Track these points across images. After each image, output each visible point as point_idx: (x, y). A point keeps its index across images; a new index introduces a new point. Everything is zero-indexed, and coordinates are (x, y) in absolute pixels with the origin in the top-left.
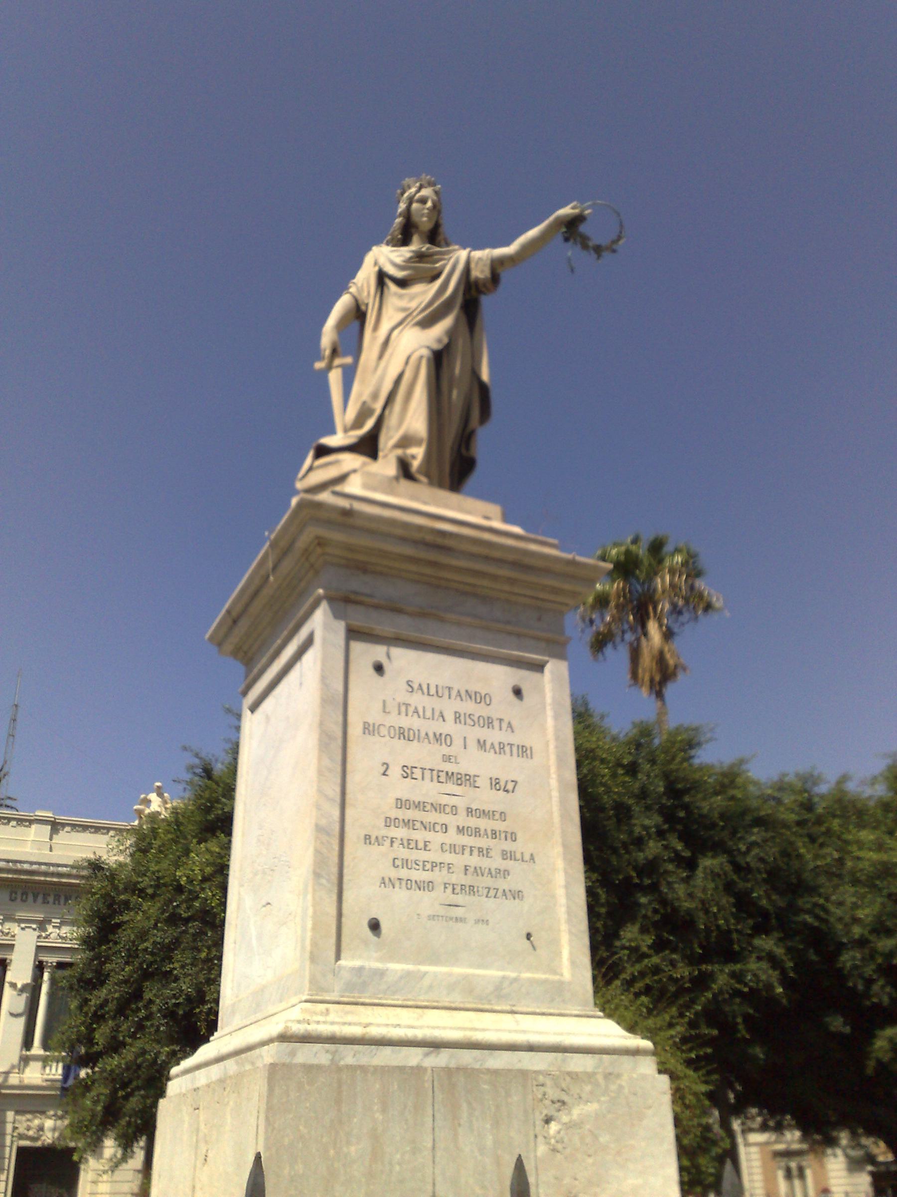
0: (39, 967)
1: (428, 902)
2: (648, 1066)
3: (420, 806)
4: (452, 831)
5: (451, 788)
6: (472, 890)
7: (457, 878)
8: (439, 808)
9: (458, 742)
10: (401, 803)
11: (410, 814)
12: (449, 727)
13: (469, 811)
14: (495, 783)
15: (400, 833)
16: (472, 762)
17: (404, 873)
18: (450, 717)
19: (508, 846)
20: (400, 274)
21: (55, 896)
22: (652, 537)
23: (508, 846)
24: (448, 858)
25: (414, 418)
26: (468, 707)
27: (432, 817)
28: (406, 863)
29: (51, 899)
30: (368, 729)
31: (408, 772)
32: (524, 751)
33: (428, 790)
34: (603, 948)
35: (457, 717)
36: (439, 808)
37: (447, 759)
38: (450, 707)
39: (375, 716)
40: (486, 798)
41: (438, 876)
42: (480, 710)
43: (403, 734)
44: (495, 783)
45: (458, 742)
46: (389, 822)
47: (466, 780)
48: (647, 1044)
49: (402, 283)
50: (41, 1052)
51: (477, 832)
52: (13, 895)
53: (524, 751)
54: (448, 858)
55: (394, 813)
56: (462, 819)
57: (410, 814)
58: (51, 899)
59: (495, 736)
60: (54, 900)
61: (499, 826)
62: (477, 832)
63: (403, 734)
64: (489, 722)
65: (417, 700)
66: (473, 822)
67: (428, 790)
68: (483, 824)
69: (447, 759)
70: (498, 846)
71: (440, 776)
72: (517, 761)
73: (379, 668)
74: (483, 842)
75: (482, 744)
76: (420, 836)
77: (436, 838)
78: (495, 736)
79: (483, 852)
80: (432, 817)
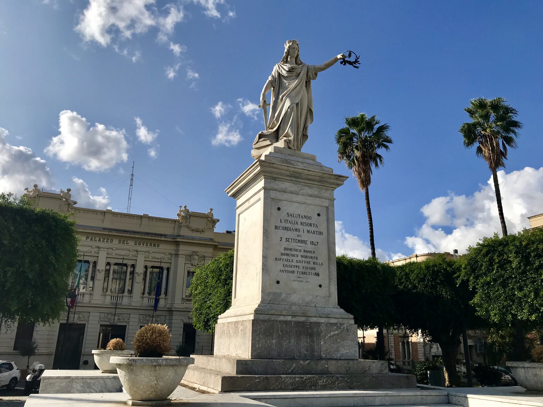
2: (352, 322)
3: (291, 250)
4: (300, 256)
5: (299, 244)
7: (301, 270)
8: (296, 250)
9: (302, 231)
11: (289, 252)
13: (304, 251)
14: (312, 243)
15: (285, 257)
16: (305, 236)
17: (286, 269)
18: (299, 223)
19: (315, 261)
23: (315, 261)
24: (298, 264)
26: (305, 220)
27: (294, 253)
28: (287, 266)
30: (276, 227)
31: (287, 240)
32: (321, 233)
33: (294, 245)
35: (301, 223)
36: (296, 250)
37: (298, 236)
38: (300, 220)
39: (279, 224)
40: (309, 247)
41: (296, 269)
42: (309, 221)
43: (285, 229)
44: (312, 243)
46: (282, 254)
47: (305, 242)
50: (147, 295)
51: (306, 257)
53: (321, 233)
54: (298, 264)
56: (302, 253)
57: (289, 252)
59: (312, 229)
61: (313, 255)
62: (306, 257)
63: (285, 229)
64: (311, 225)
65: (290, 219)
66: (306, 254)
67: (294, 245)
68: (308, 254)
69: (298, 236)
71: (295, 240)
72: (319, 236)
74: (308, 260)
75: (308, 232)
76: (290, 258)
77: (295, 259)
78: (312, 229)
79: (308, 263)
80: (294, 253)
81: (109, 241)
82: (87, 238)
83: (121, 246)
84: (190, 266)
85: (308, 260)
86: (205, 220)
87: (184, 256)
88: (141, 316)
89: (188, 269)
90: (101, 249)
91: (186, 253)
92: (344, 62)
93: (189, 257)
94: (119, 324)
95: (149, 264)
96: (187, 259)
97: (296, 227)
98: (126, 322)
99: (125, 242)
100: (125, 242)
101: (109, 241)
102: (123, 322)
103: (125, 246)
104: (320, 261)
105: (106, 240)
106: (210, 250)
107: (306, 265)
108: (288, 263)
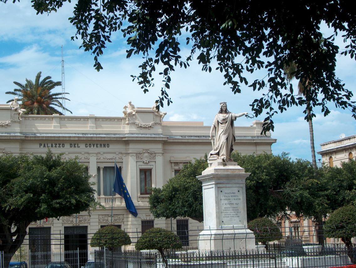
0: (99, 169)
1: (228, 219)
3: (227, 208)
6: (233, 217)
7: (232, 215)
9: (231, 199)
10: (225, 208)
11: (226, 209)
12: (231, 198)
14: (236, 204)
15: (225, 211)
16: (233, 202)
18: (230, 196)
19: (238, 211)
20: (221, 122)
21: (100, 144)
22: (321, 32)
23: (238, 211)
24: (231, 213)
25: (224, 152)
26: (233, 195)
27: (229, 209)
29: (99, 146)
32: (240, 199)
34: (308, 167)
35: (231, 196)
37: (230, 202)
38: (230, 195)
40: (235, 206)
41: (229, 216)
42: (234, 195)
44: (236, 204)
45: (231, 199)
47: (233, 204)
48: (253, 232)
49: (221, 124)
52: (86, 145)
53: (240, 199)
54: (231, 213)
55: (224, 209)
57: (226, 209)
58: (99, 146)
60: (100, 146)
61: (236, 209)
64: (235, 196)
69: (230, 202)
70: (236, 211)
73: (221, 191)
77: (229, 211)
78: (236, 198)
80: (229, 209)
81: (61, 145)
82: (41, 145)
83: (73, 149)
84: (141, 163)
85: (235, 211)
86: (152, 115)
87: (135, 155)
88: (101, 217)
89: (140, 167)
90: (91, 155)
91: (135, 151)
92: (246, 116)
93: (138, 155)
94: (81, 225)
95: (102, 166)
96: (137, 157)
97: (229, 198)
98: (88, 223)
99: (76, 146)
100: (76, 146)
101: (61, 145)
102: (84, 223)
103: (76, 150)
104: (239, 211)
105: (58, 146)
106: (160, 146)
107: (234, 213)
108: (226, 214)
